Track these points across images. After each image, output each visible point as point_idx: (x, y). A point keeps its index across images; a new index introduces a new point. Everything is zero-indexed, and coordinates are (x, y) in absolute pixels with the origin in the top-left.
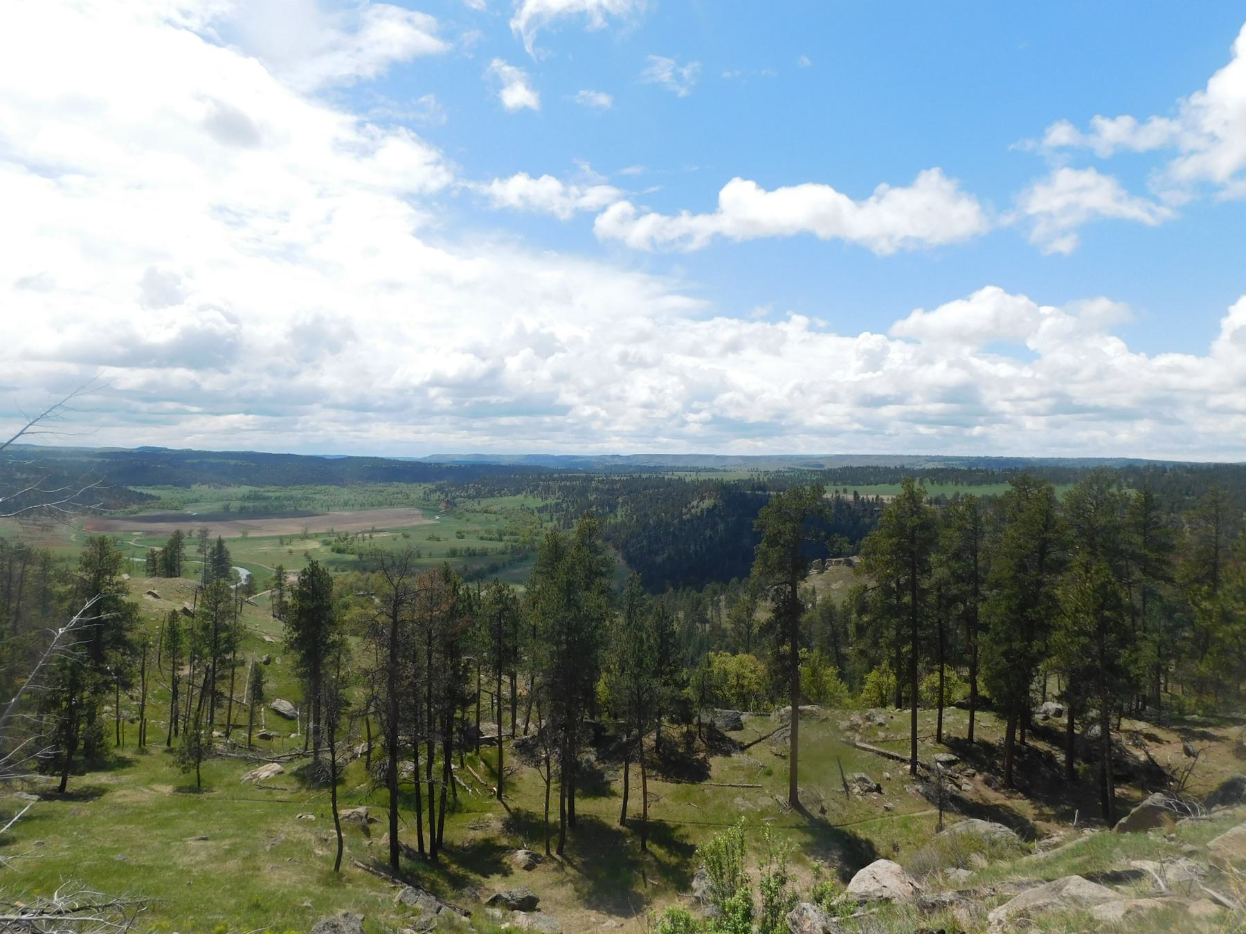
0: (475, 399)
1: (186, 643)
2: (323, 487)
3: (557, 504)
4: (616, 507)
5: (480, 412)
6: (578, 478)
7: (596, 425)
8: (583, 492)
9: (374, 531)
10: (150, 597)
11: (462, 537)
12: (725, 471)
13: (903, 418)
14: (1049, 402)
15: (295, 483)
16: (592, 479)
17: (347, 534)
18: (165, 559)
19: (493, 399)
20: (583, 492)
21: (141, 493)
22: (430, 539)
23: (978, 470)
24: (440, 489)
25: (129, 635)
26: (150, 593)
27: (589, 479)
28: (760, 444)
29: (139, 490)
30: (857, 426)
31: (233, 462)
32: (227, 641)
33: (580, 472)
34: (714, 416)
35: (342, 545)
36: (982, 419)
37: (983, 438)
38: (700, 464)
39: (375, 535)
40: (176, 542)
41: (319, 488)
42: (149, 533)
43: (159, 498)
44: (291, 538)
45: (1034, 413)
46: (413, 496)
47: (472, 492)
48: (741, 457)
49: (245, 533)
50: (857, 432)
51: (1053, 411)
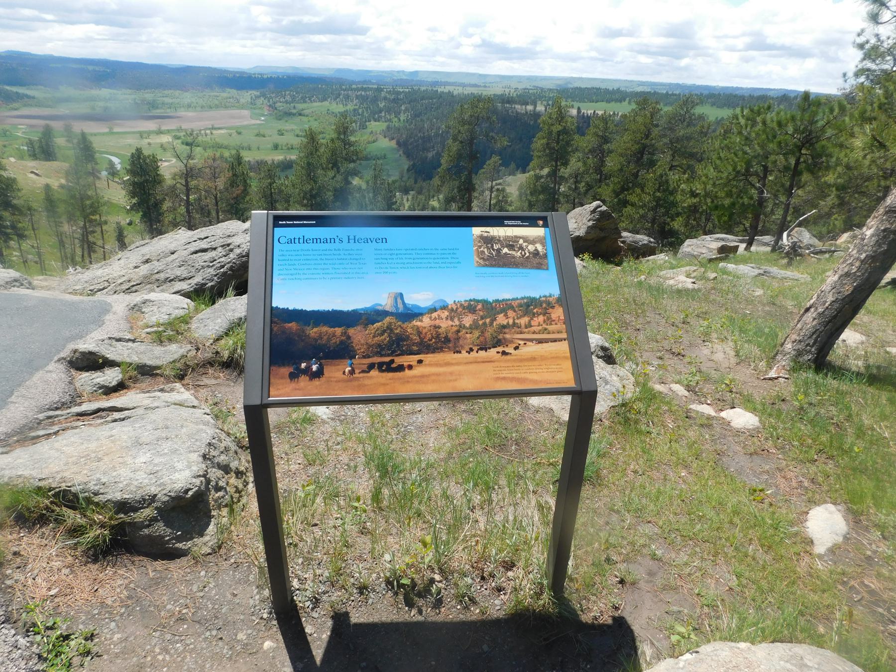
0: (292, 18)
1: (61, 208)
2: (170, 92)
3: (355, 110)
4: (399, 113)
5: (297, 30)
6: (371, 89)
7: (388, 45)
8: (375, 100)
9: (213, 128)
10: (32, 175)
11: (282, 135)
12: (485, 87)
13: (631, 49)
14: (748, 40)
15: (146, 88)
16: (382, 90)
17: (193, 131)
18: (41, 147)
19: (306, 19)
20: (375, 100)
21: (17, 93)
22: (257, 135)
23: (673, 95)
24: (263, 95)
25: (15, 202)
26: (32, 172)
27: (379, 90)
28: (516, 66)
29: (14, 89)
30: (594, 54)
31: (90, 68)
32: (92, 206)
33: (373, 84)
34: (483, 40)
35: (189, 140)
36: (692, 53)
37: (687, 68)
38: (466, 81)
39: (214, 132)
40: (48, 133)
41: (166, 92)
42: (32, 126)
43: (34, 98)
44: (149, 133)
45: (732, 49)
46: (242, 101)
47: (288, 98)
48: (499, 76)
49: (111, 129)
50: (593, 59)
51: (750, 47)
